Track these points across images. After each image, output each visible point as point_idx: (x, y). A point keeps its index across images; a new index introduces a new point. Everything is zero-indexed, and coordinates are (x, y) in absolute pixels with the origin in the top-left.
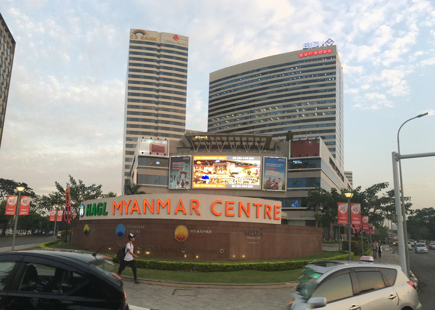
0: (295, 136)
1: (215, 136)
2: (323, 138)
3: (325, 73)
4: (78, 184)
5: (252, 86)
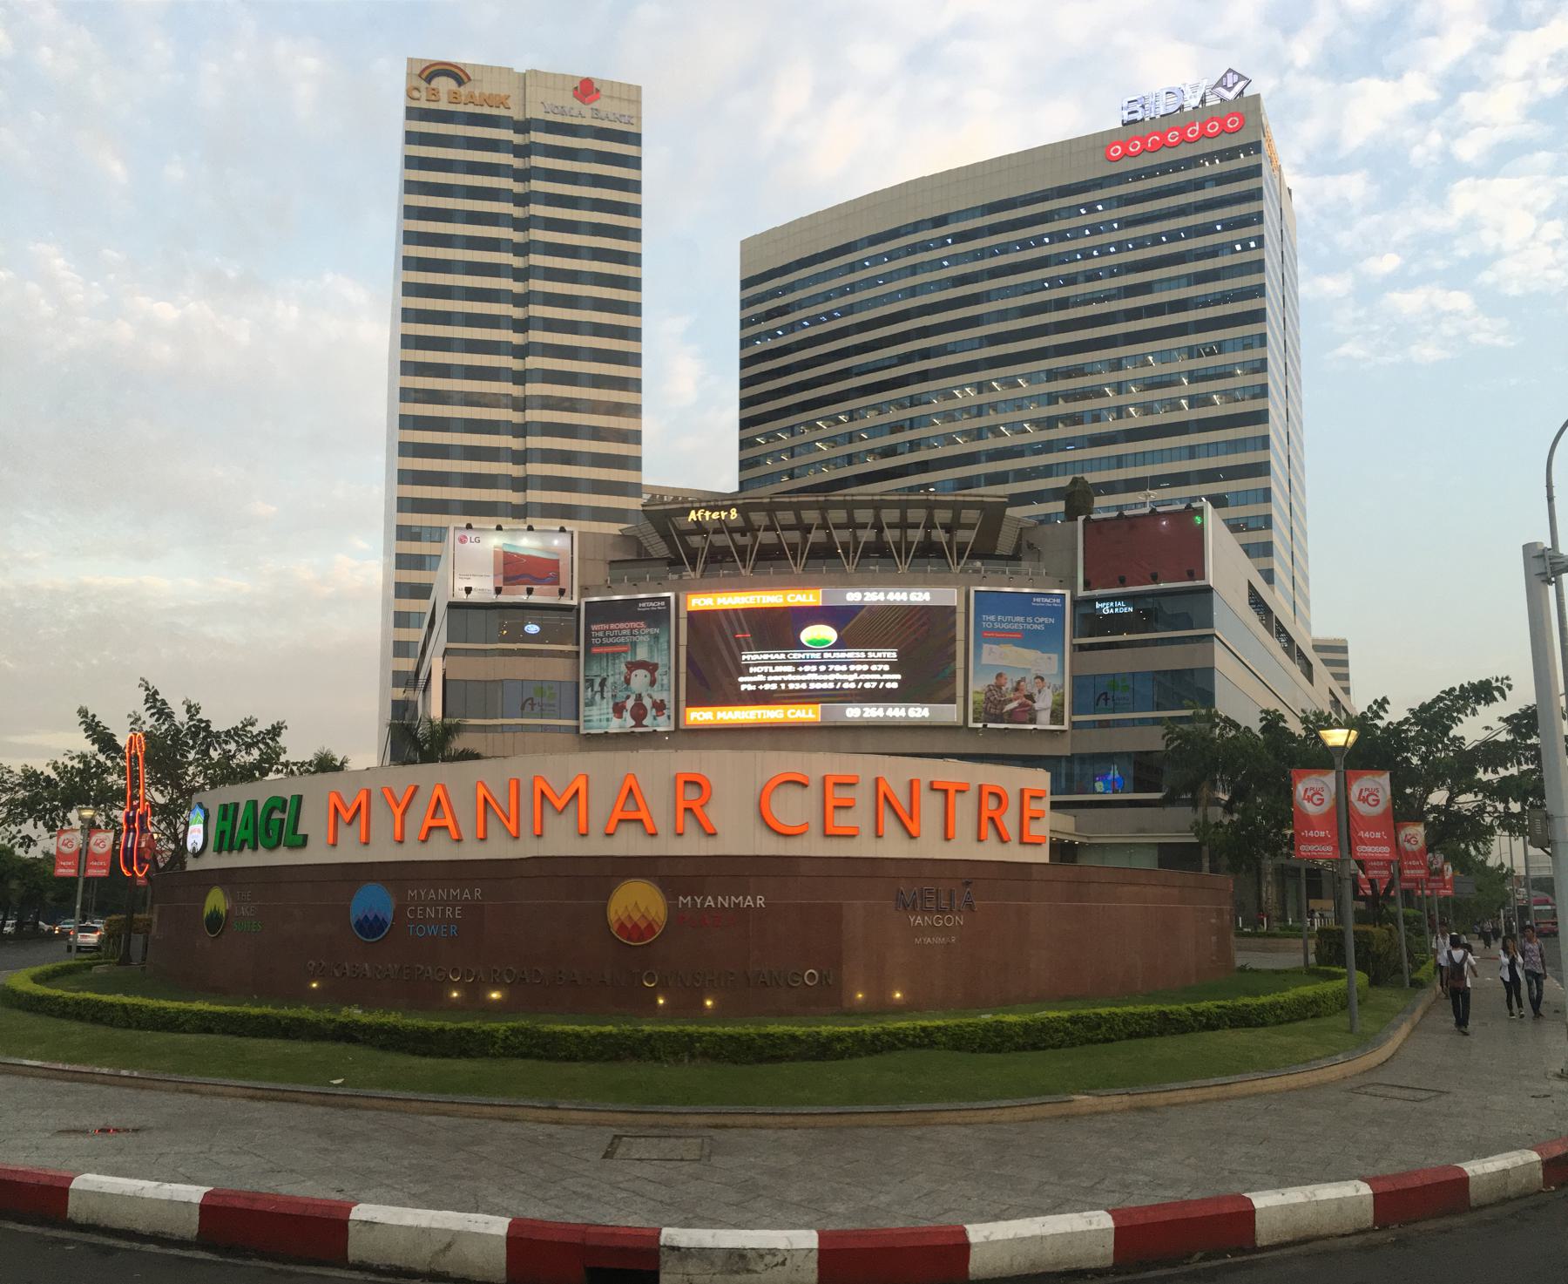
0: (1100, 501)
1: (771, 508)
2: (1218, 501)
3: (1215, 223)
4: (181, 717)
5: (912, 292)
